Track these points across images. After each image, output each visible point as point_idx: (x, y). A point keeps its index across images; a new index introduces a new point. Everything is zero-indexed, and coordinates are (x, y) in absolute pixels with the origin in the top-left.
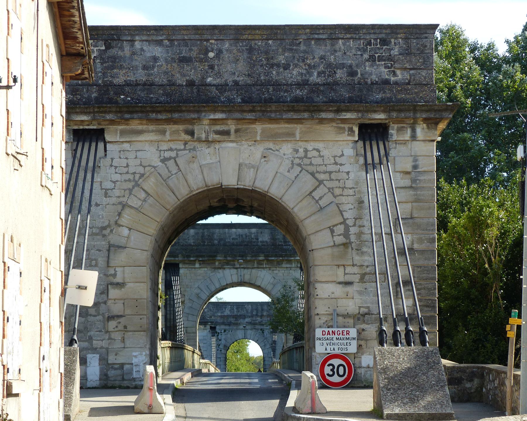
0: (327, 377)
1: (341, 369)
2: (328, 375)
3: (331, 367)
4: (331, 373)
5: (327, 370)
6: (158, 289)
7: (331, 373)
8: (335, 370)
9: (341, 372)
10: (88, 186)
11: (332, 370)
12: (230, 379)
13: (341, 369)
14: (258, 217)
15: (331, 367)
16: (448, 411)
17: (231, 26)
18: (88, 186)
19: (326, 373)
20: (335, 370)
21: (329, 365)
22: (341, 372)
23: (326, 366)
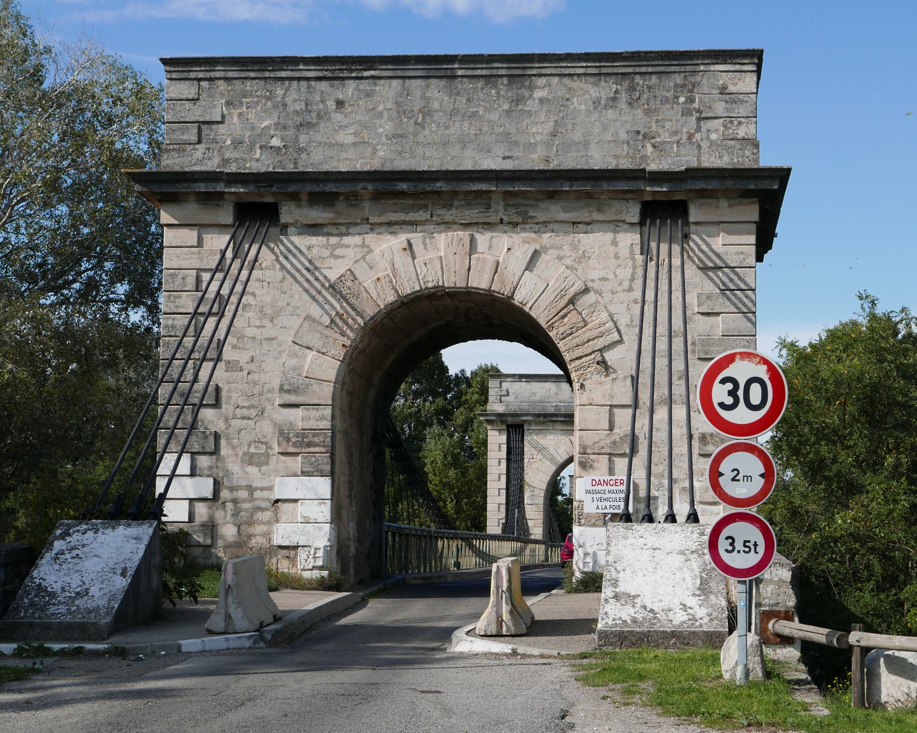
0: (761, 549)
1: (756, 389)
2: (722, 405)
3: (729, 386)
4: (729, 401)
5: (720, 393)
6: (62, 650)
7: (729, 401)
8: (740, 393)
9: (756, 398)
10: (677, 295)
11: (733, 393)
12: (77, 685)
13: (756, 389)
14: (879, 667)
15: (729, 386)
16: (218, 189)
17: (245, 58)
18: (677, 295)
19: (716, 400)
20: (740, 393)
21: (724, 381)
22: (756, 398)
23: (716, 384)
